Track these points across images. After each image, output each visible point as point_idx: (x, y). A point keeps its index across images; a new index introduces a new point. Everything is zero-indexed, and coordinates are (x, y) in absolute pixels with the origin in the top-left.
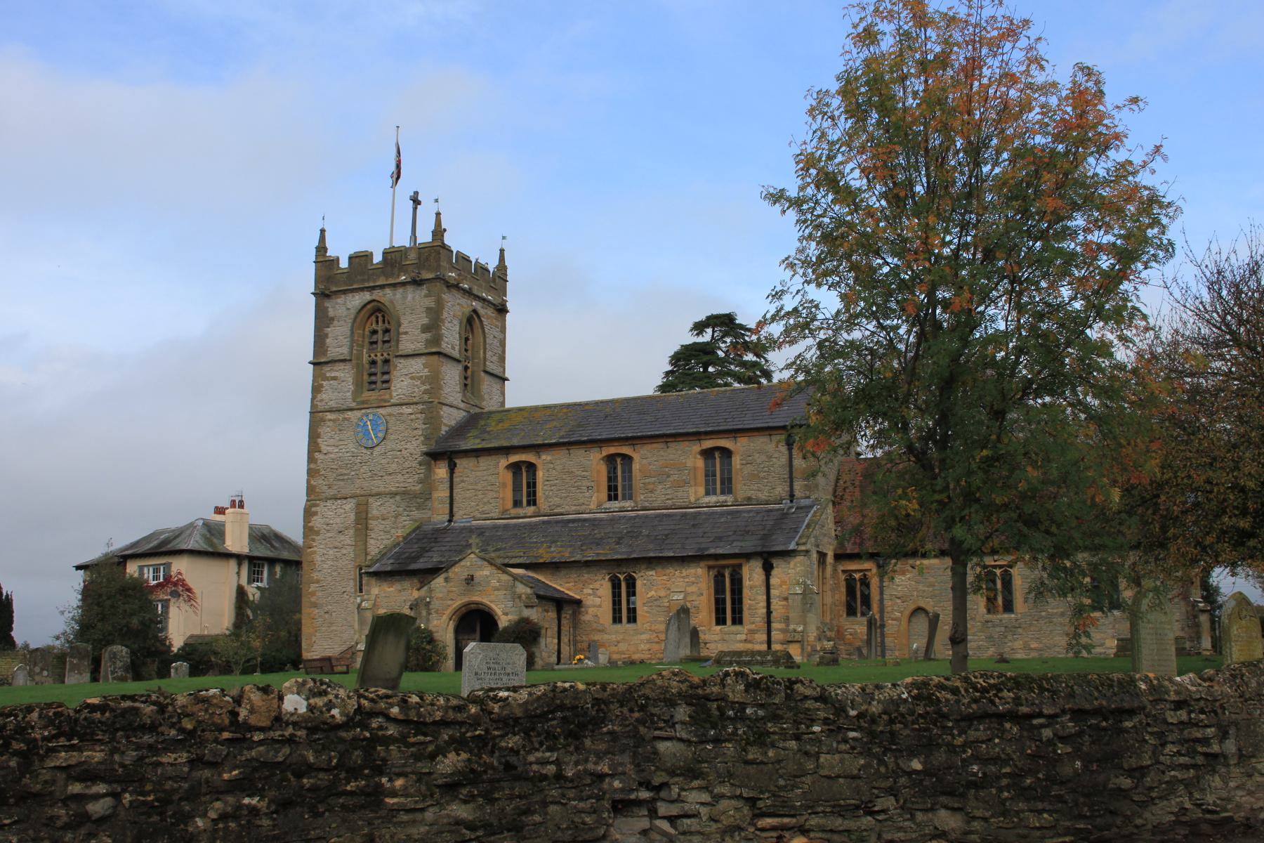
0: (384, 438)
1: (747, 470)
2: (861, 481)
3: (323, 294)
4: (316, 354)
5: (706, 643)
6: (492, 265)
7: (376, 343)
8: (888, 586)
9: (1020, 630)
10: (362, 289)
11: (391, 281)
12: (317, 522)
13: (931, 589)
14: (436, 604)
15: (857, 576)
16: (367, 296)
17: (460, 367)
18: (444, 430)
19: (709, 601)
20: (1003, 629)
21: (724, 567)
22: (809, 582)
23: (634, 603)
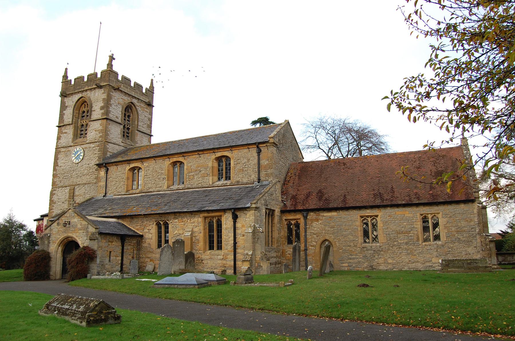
0: (83, 159)
1: (238, 167)
2: (299, 173)
3: (64, 95)
4: (59, 123)
5: (202, 260)
6: (146, 85)
7: (84, 116)
8: (309, 228)
9: (382, 252)
10: (78, 92)
11: (90, 88)
12: (55, 198)
13: (332, 229)
14: (52, 238)
15: (293, 222)
16: (80, 95)
17: (122, 127)
18: (109, 154)
19: (205, 236)
20: (372, 252)
21: (213, 217)
22: (257, 226)
23: (168, 237)
